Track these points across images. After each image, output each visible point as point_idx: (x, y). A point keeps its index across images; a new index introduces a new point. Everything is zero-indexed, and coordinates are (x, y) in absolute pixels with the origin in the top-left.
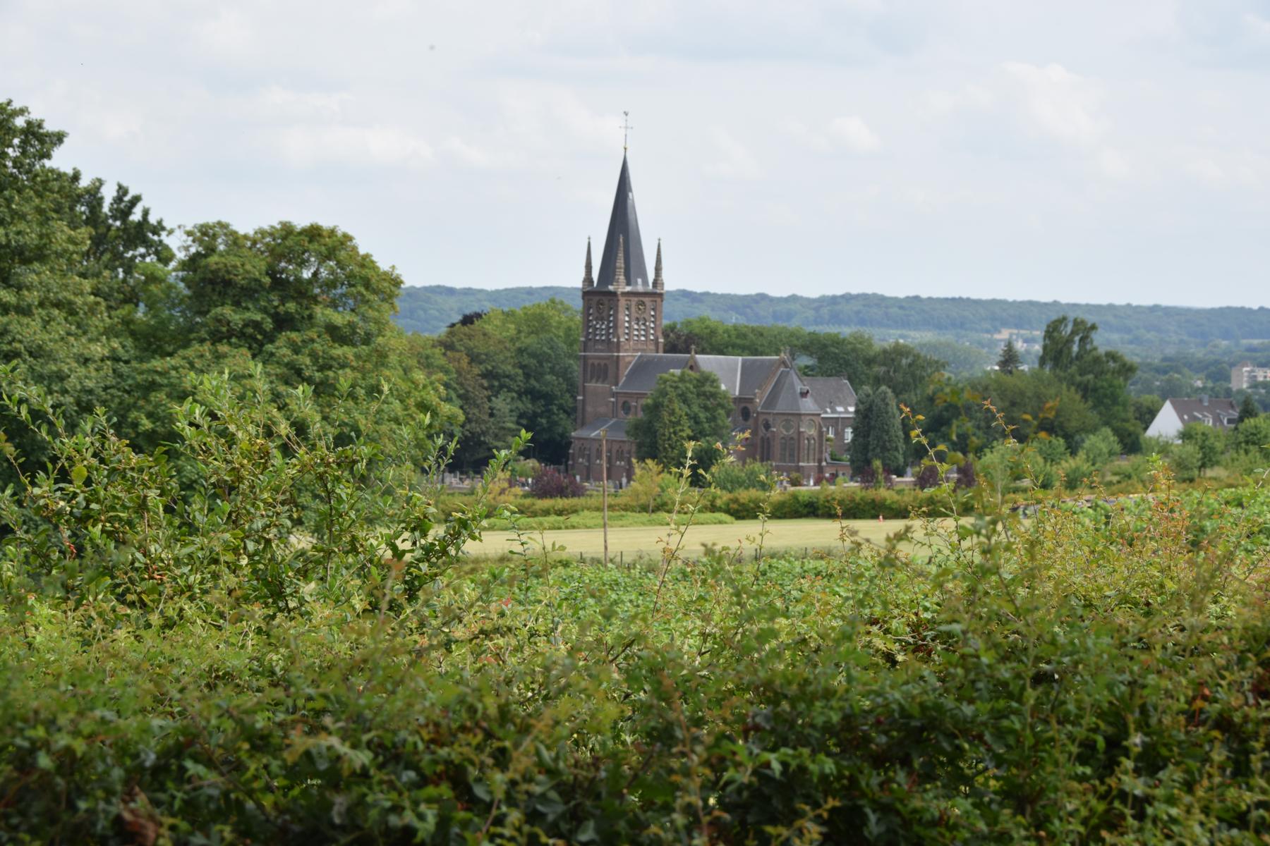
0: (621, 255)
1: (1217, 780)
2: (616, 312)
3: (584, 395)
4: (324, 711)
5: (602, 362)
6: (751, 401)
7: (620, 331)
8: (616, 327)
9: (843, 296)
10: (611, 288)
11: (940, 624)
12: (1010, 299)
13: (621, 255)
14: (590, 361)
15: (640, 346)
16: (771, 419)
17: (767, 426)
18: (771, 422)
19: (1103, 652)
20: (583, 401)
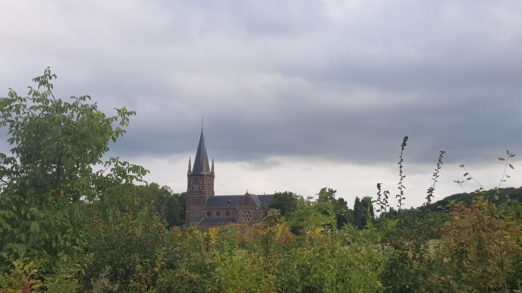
7: (205, 188)
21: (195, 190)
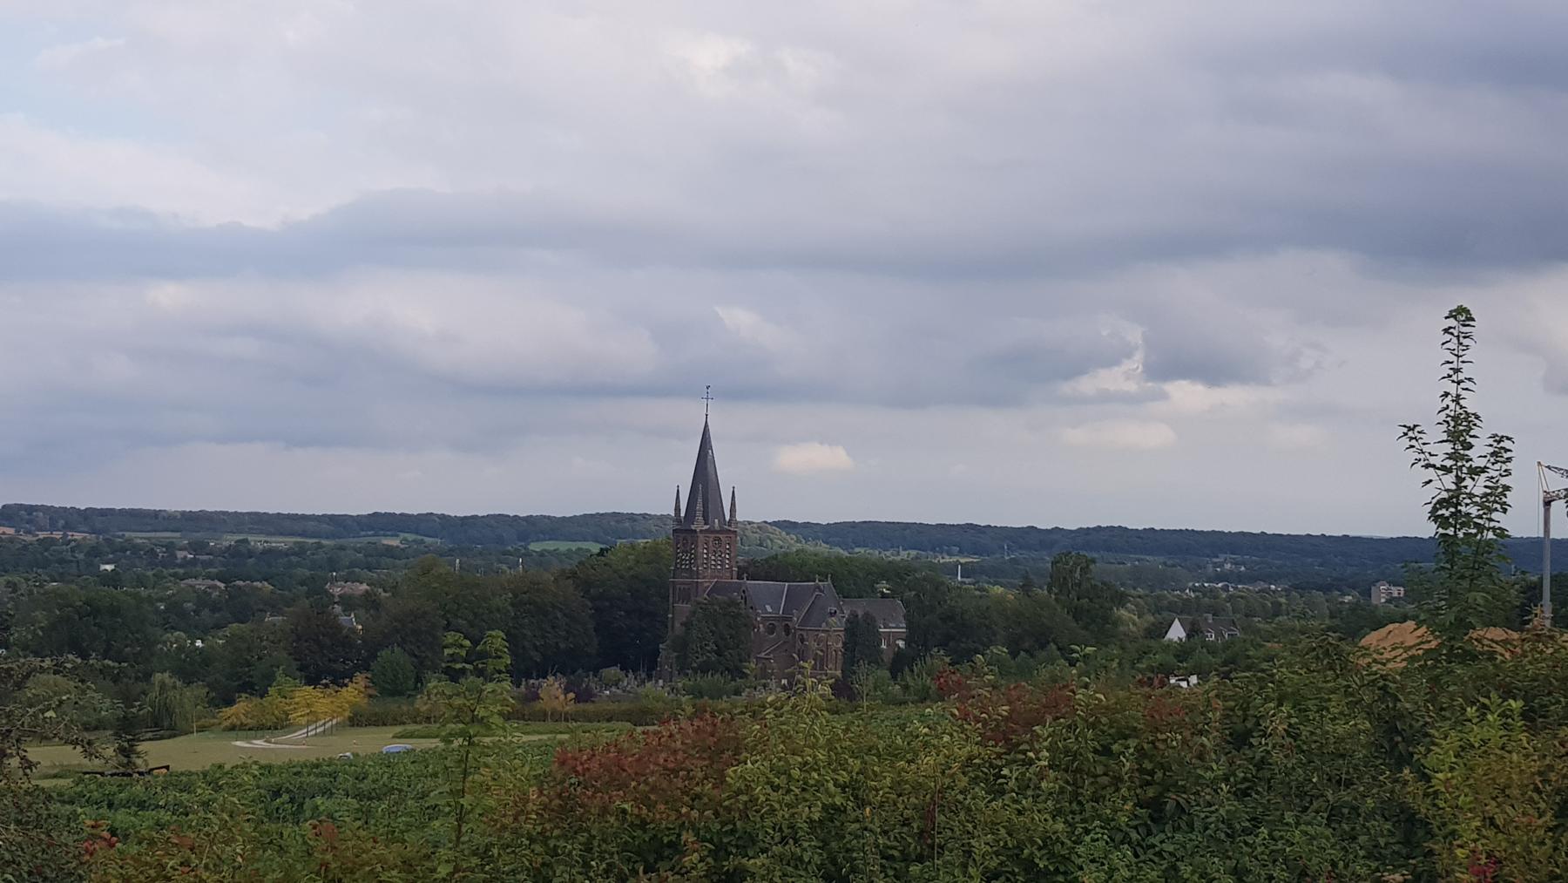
0: (700, 500)
1: (419, 868)
2: (697, 546)
3: (673, 614)
4: (693, 826)
5: (686, 587)
6: (790, 619)
7: (699, 562)
8: (695, 559)
9: (1094, 529)
10: (693, 527)
11: (1225, 832)
12: (398, 512)
13: (700, 500)
14: (678, 586)
15: (717, 574)
16: (804, 634)
17: (802, 640)
18: (805, 637)
19: (1001, 840)
20: (673, 618)
21: (683, 567)
